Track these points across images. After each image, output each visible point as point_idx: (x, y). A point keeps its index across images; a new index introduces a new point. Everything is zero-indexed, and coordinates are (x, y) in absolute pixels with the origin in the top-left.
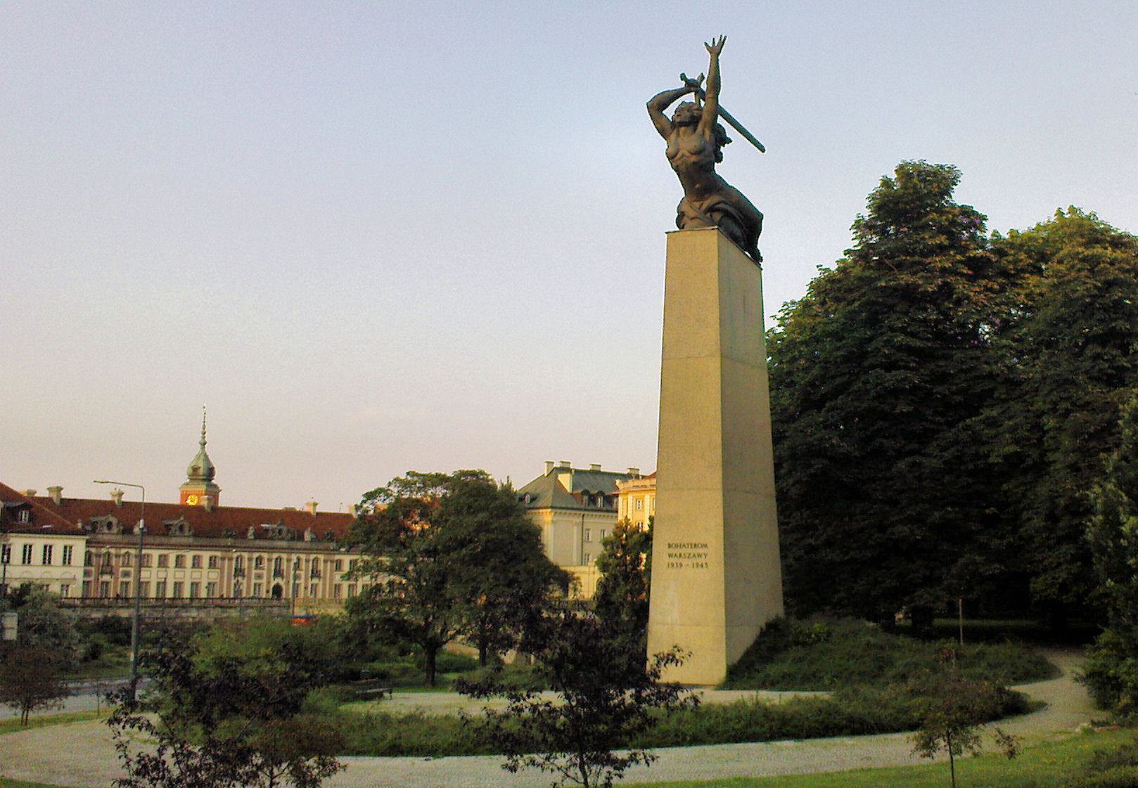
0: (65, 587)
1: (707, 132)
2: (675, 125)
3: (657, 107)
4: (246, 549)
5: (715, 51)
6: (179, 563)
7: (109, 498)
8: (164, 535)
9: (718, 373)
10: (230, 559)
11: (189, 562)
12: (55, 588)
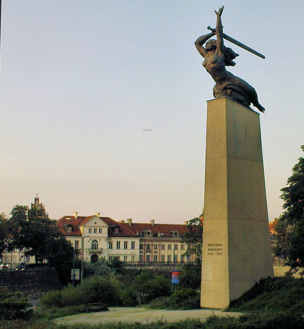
0: (125, 257)
1: (220, 52)
2: (207, 50)
3: (200, 43)
5: (220, 14)
7: (150, 223)
8: (170, 237)
9: (226, 165)
12: (129, 259)
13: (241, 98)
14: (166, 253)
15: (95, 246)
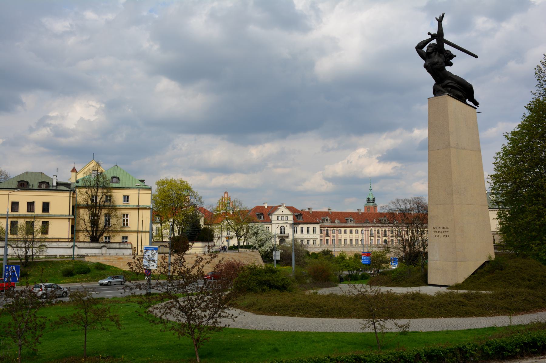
3: (419, 48)
4: (374, 227)
5: (440, 20)
6: (351, 232)
10: (368, 231)
11: (354, 232)
13: (460, 94)
14: (342, 237)
15: (282, 231)
